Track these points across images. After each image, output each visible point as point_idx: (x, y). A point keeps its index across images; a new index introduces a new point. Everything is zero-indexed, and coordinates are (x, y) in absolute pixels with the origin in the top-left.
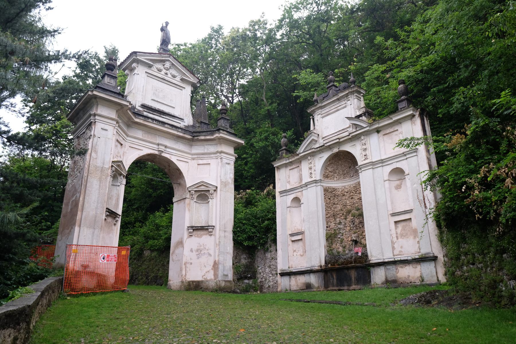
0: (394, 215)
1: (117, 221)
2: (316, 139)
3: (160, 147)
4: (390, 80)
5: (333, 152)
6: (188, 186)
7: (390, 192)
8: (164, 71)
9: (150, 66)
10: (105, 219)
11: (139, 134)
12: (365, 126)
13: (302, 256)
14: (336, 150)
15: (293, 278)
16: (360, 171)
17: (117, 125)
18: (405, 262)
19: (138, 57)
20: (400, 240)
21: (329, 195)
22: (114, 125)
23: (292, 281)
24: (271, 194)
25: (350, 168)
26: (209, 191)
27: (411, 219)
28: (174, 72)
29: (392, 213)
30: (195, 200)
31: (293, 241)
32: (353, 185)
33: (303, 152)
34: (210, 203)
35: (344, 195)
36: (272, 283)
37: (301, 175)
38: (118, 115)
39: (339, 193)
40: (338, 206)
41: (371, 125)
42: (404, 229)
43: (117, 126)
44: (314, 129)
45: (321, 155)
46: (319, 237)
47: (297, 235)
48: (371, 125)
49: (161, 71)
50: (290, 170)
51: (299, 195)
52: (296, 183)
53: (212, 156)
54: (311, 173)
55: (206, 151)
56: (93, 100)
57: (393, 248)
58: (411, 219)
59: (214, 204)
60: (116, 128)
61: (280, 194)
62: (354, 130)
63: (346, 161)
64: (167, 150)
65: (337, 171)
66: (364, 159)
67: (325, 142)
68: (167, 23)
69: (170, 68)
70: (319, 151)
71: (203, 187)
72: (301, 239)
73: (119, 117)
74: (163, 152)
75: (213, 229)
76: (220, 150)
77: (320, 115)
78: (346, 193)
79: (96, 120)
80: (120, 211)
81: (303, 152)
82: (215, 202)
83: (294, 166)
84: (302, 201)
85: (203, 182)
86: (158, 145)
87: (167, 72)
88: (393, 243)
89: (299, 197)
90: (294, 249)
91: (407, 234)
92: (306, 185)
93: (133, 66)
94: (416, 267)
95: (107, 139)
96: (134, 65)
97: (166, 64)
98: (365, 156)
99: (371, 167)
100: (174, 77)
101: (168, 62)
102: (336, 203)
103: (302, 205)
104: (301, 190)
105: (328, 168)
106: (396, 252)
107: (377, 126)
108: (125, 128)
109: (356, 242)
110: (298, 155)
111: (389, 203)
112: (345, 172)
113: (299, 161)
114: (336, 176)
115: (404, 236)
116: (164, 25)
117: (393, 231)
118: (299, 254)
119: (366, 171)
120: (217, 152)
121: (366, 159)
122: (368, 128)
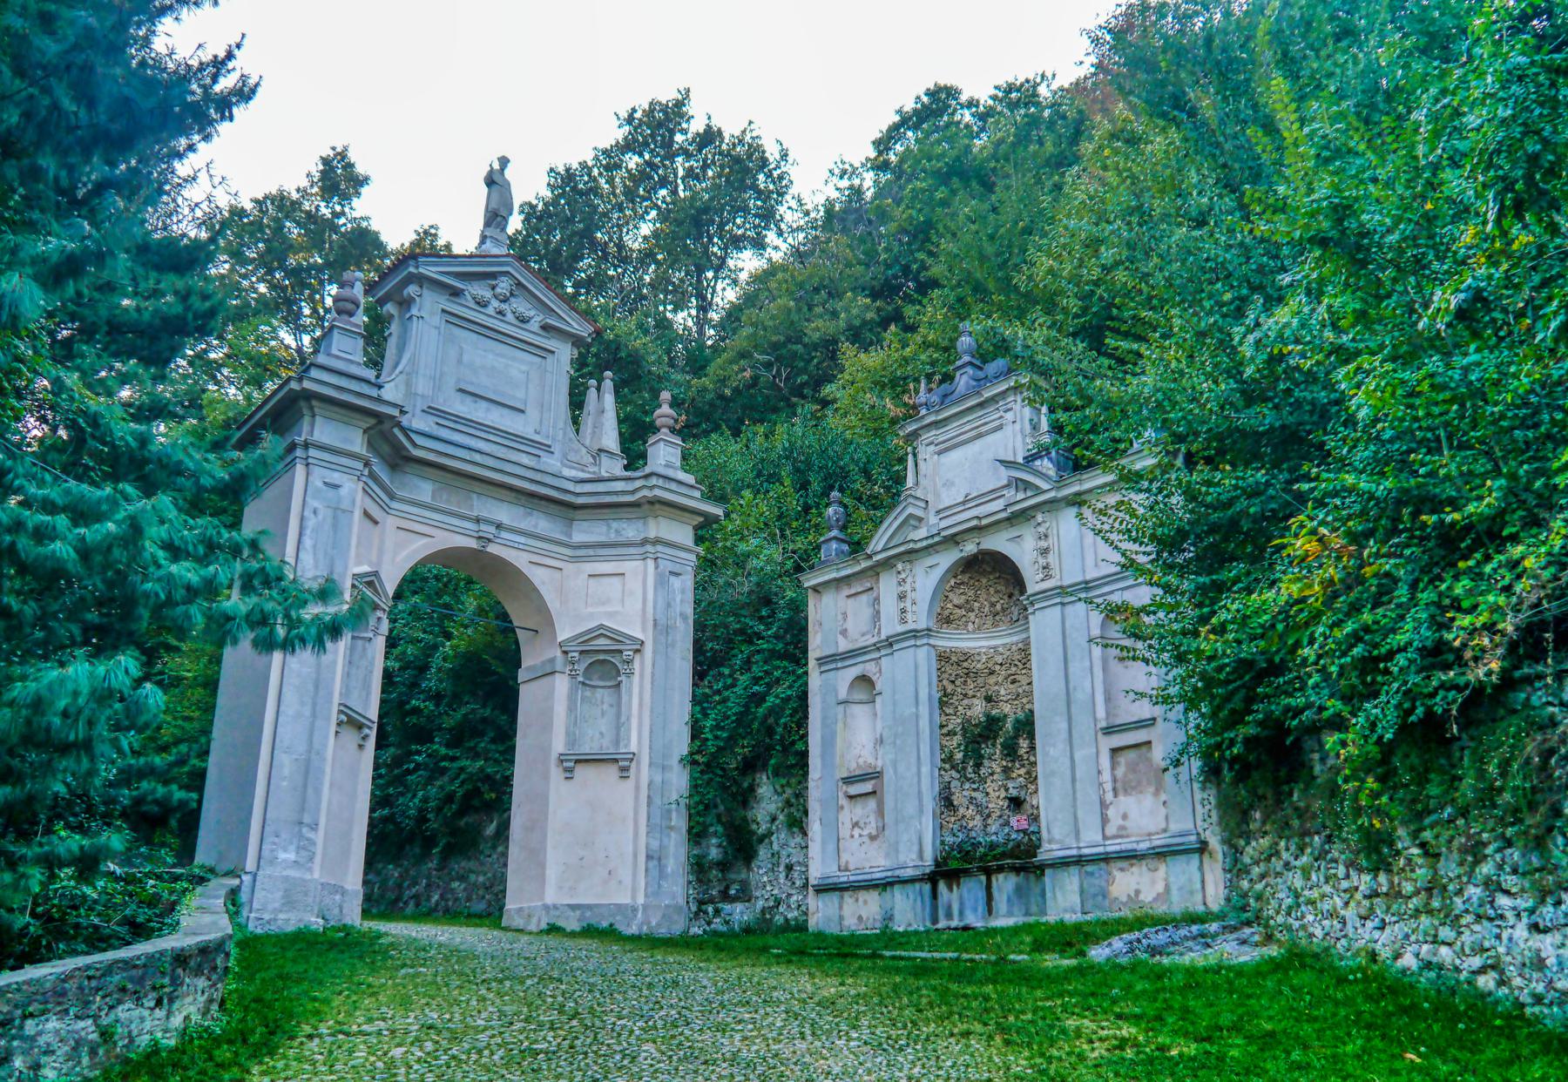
0: (1109, 731)
1: (365, 738)
2: (920, 513)
3: (483, 527)
4: (1021, 549)
6: (562, 636)
7: (1105, 669)
8: (495, 303)
9: (456, 293)
11: (424, 490)
12: (1045, 486)
13: (873, 838)
14: (970, 548)
17: (366, 472)
23: (845, 907)
25: (1010, 596)
26: (620, 652)
28: (521, 305)
29: (1104, 724)
31: (851, 797)
33: (884, 550)
34: (623, 686)
35: (992, 673)
38: (369, 442)
40: (976, 701)
41: (1060, 483)
42: (1132, 768)
44: (917, 484)
45: (930, 561)
48: (1060, 483)
49: (485, 306)
51: (870, 669)
53: (632, 550)
54: (903, 611)
55: (613, 537)
56: (302, 404)
57: (1105, 821)
58: (1149, 743)
59: (636, 690)
61: (820, 665)
62: (1021, 496)
64: (504, 535)
67: (944, 524)
68: (504, 161)
70: (926, 548)
71: (602, 641)
76: (652, 534)
77: (932, 448)
80: (373, 713)
81: (884, 550)
82: (639, 686)
85: (601, 627)
86: (478, 520)
87: (504, 306)
88: (1104, 805)
92: (890, 643)
93: (405, 293)
96: (412, 290)
99: (1058, 600)
100: (523, 320)
102: (971, 693)
105: (951, 595)
106: (1111, 830)
107: (1076, 488)
108: (384, 476)
111: (1100, 698)
112: (998, 607)
115: (1133, 788)
116: (496, 166)
117: (1106, 776)
118: (865, 832)
121: (1048, 577)
122: (1052, 494)
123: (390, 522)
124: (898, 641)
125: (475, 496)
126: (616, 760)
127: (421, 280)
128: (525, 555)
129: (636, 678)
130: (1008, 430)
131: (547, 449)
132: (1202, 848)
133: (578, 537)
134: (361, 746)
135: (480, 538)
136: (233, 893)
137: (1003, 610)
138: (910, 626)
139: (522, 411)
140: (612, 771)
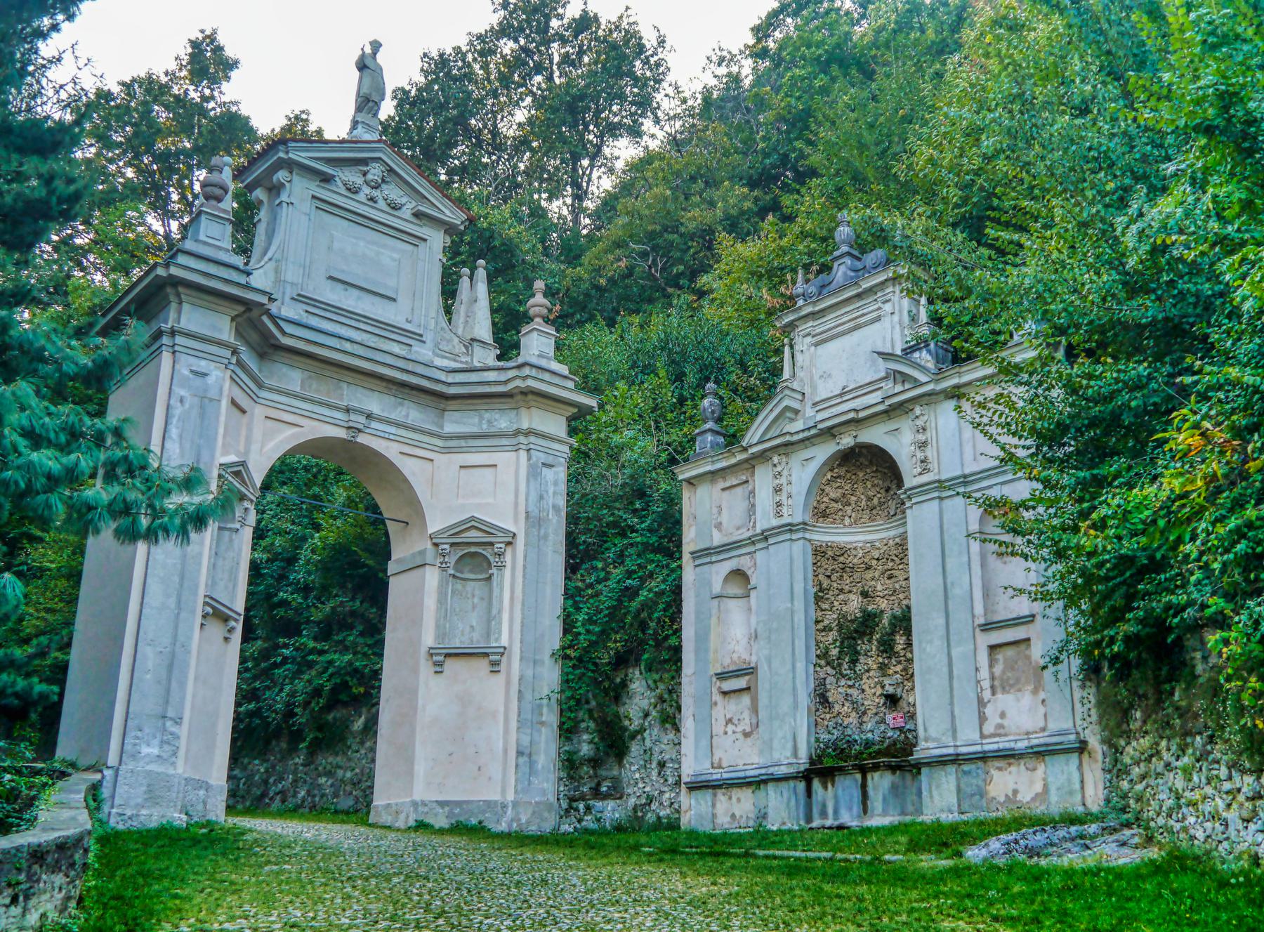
0: (987, 627)
1: (231, 630)
3: (353, 417)
5: (841, 447)
6: (430, 531)
8: (367, 190)
9: (326, 179)
10: (202, 625)
12: (924, 379)
13: (746, 735)
14: (847, 441)
15: (721, 796)
16: (908, 504)
18: (1009, 756)
19: (291, 155)
20: (999, 696)
21: (828, 565)
22: (226, 361)
24: (1242, 131)
25: (887, 490)
26: (492, 544)
27: (1028, 640)
28: (393, 192)
30: (451, 571)
31: (725, 693)
32: (894, 538)
34: (495, 577)
35: (868, 568)
36: (668, 811)
37: (753, 505)
39: (855, 561)
40: (852, 596)
41: (939, 375)
42: (1010, 666)
43: (234, 360)
46: (794, 682)
47: (737, 676)
48: (939, 375)
49: (356, 192)
50: (723, 490)
51: (744, 563)
52: (738, 529)
53: (504, 442)
54: (779, 504)
56: (169, 290)
58: (1028, 640)
60: (232, 367)
62: (899, 388)
63: (876, 471)
64: (374, 425)
65: (853, 498)
66: (919, 470)
67: (820, 417)
68: (376, 46)
69: (383, 181)
70: (802, 441)
72: (748, 689)
73: (239, 333)
74: (360, 431)
75: (502, 654)
77: (809, 339)
78: (874, 562)
79: (177, 348)
83: (733, 481)
84: (753, 582)
85: (473, 518)
87: (375, 193)
88: (981, 703)
89: (744, 569)
90: (728, 716)
91: (1018, 681)
92: (765, 536)
93: (275, 178)
94: (1034, 769)
95: (206, 401)
96: (282, 175)
97: (373, 171)
98: (922, 462)
99: (936, 494)
100: (395, 207)
101: (374, 165)
102: (847, 588)
103: (753, 593)
104: (751, 549)
105: (827, 489)
106: (989, 728)
109: (892, 701)
110: (745, 449)
112: (875, 501)
113: (751, 464)
114: (849, 512)
115: (1011, 686)
116: (368, 50)
117: (984, 674)
118: (740, 729)
119: (925, 505)
120: (518, 432)
121: (925, 471)
122: (931, 387)
123: (259, 412)
124: (773, 535)
125: (345, 386)
126: (487, 655)
127: (291, 165)
128: (395, 445)
129: (507, 572)
130: (886, 322)
131: (419, 338)
132: (1082, 748)
133: (449, 428)
134: (226, 639)
135: (349, 428)
136: (95, 789)
137: (880, 504)
138: (786, 520)
139: (394, 300)
140: (483, 664)
